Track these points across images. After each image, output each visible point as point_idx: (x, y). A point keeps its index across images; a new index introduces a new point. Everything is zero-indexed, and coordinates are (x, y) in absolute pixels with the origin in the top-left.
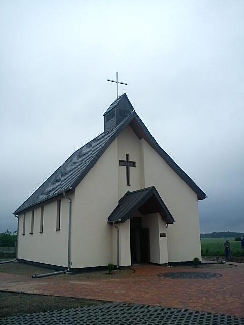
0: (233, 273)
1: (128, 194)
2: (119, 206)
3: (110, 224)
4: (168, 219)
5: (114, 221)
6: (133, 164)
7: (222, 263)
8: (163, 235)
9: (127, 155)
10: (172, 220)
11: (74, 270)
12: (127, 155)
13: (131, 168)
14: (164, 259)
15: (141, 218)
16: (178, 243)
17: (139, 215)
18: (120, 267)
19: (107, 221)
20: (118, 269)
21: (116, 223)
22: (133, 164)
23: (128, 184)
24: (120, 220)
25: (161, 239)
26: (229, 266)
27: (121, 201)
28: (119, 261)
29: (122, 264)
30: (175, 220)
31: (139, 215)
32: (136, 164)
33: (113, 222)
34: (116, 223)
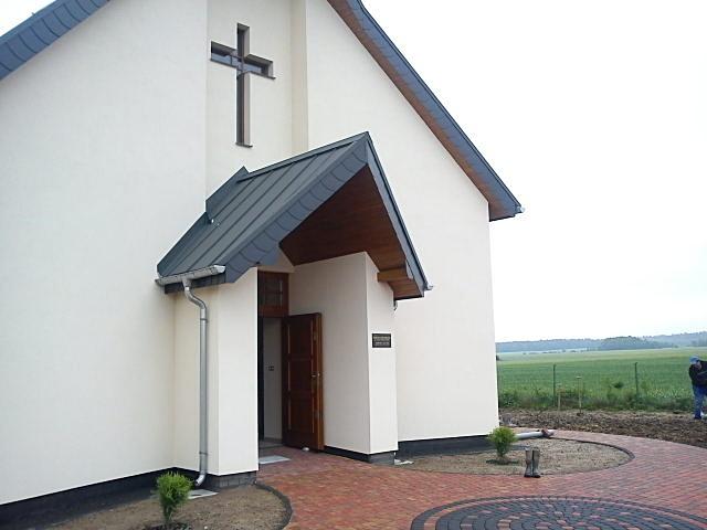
0: (658, 469)
1: (242, 179)
2: (205, 220)
3: (171, 289)
4: (403, 280)
5: (185, 276)
6: (264, 67)
7: (545, 436)
8: (382, 341)
9: (242, 32)
10: (420, 284)
11: (470, 170)
12: (242, 32)
13: (255, 82)
14: (382, 440)
15: (284, 277)
16: (414, 378)
17: (283, 265)
18: (211, 482)
19: (156, 276)
20: (204, 486)
21: (198, 283)
22: (264, 67)
23: (241, 140)
24: (221, 269)
25: (375, 354)
26: (575, 446)
27: (217, 203)
28: (204, 454)
29: (222, 466)
30: (429, 284)
31: (283, 265)
32: (276, 70)
33: (185, 279)
34: (198, 283)
